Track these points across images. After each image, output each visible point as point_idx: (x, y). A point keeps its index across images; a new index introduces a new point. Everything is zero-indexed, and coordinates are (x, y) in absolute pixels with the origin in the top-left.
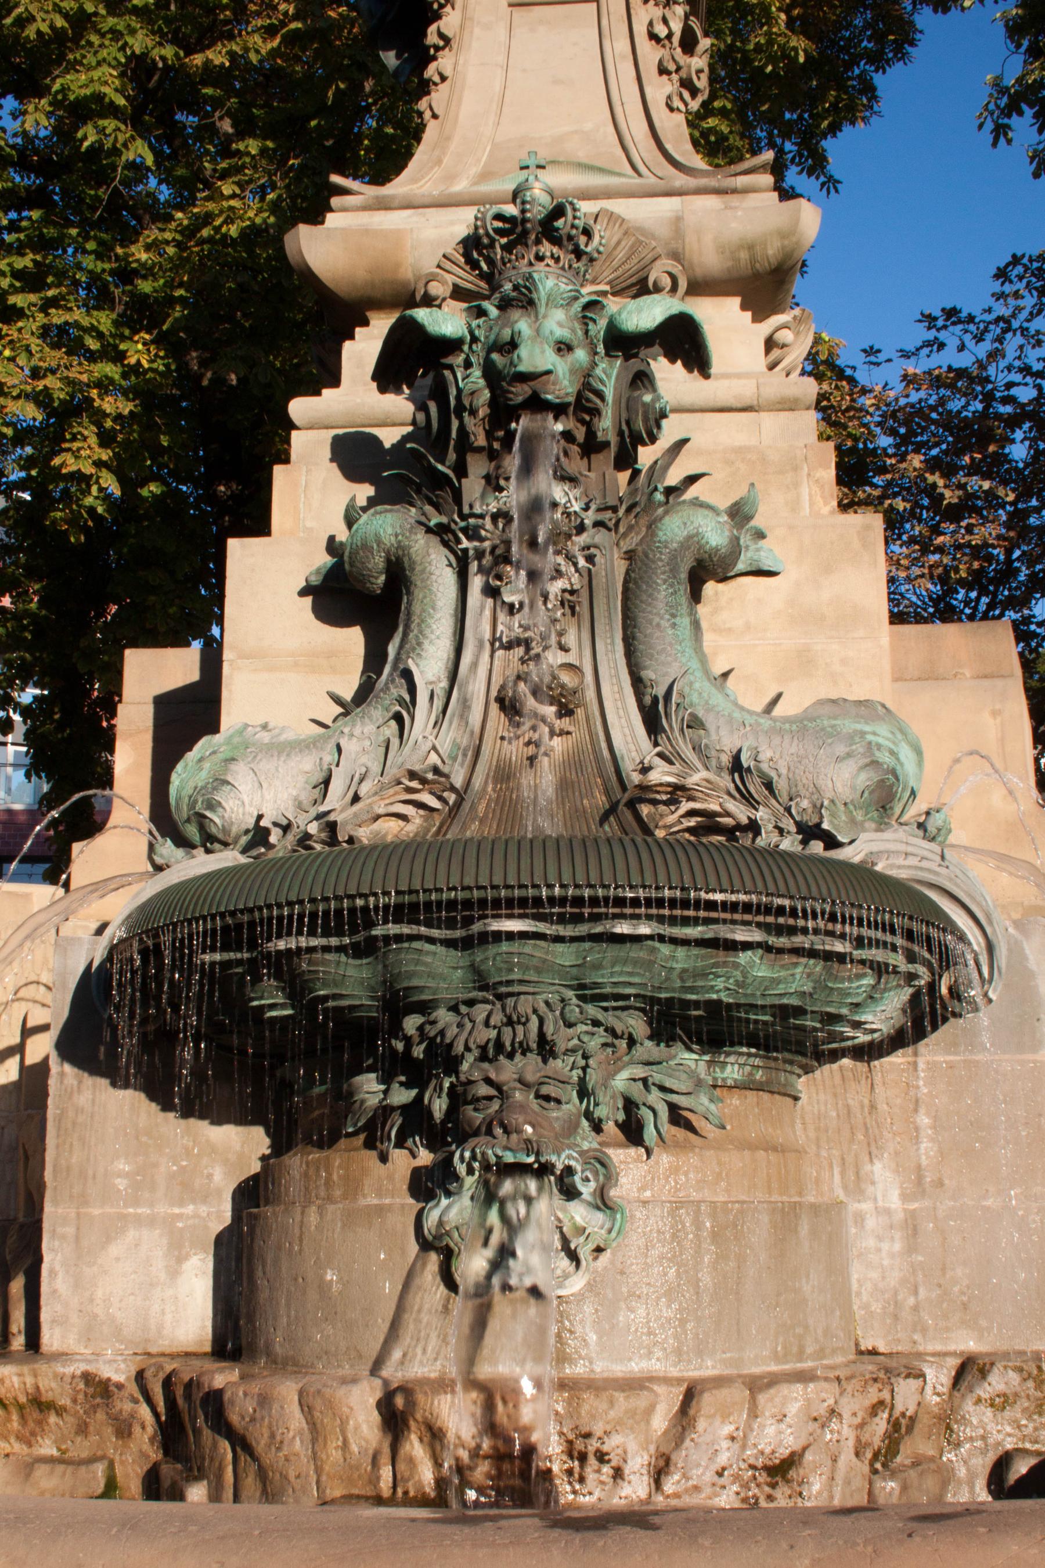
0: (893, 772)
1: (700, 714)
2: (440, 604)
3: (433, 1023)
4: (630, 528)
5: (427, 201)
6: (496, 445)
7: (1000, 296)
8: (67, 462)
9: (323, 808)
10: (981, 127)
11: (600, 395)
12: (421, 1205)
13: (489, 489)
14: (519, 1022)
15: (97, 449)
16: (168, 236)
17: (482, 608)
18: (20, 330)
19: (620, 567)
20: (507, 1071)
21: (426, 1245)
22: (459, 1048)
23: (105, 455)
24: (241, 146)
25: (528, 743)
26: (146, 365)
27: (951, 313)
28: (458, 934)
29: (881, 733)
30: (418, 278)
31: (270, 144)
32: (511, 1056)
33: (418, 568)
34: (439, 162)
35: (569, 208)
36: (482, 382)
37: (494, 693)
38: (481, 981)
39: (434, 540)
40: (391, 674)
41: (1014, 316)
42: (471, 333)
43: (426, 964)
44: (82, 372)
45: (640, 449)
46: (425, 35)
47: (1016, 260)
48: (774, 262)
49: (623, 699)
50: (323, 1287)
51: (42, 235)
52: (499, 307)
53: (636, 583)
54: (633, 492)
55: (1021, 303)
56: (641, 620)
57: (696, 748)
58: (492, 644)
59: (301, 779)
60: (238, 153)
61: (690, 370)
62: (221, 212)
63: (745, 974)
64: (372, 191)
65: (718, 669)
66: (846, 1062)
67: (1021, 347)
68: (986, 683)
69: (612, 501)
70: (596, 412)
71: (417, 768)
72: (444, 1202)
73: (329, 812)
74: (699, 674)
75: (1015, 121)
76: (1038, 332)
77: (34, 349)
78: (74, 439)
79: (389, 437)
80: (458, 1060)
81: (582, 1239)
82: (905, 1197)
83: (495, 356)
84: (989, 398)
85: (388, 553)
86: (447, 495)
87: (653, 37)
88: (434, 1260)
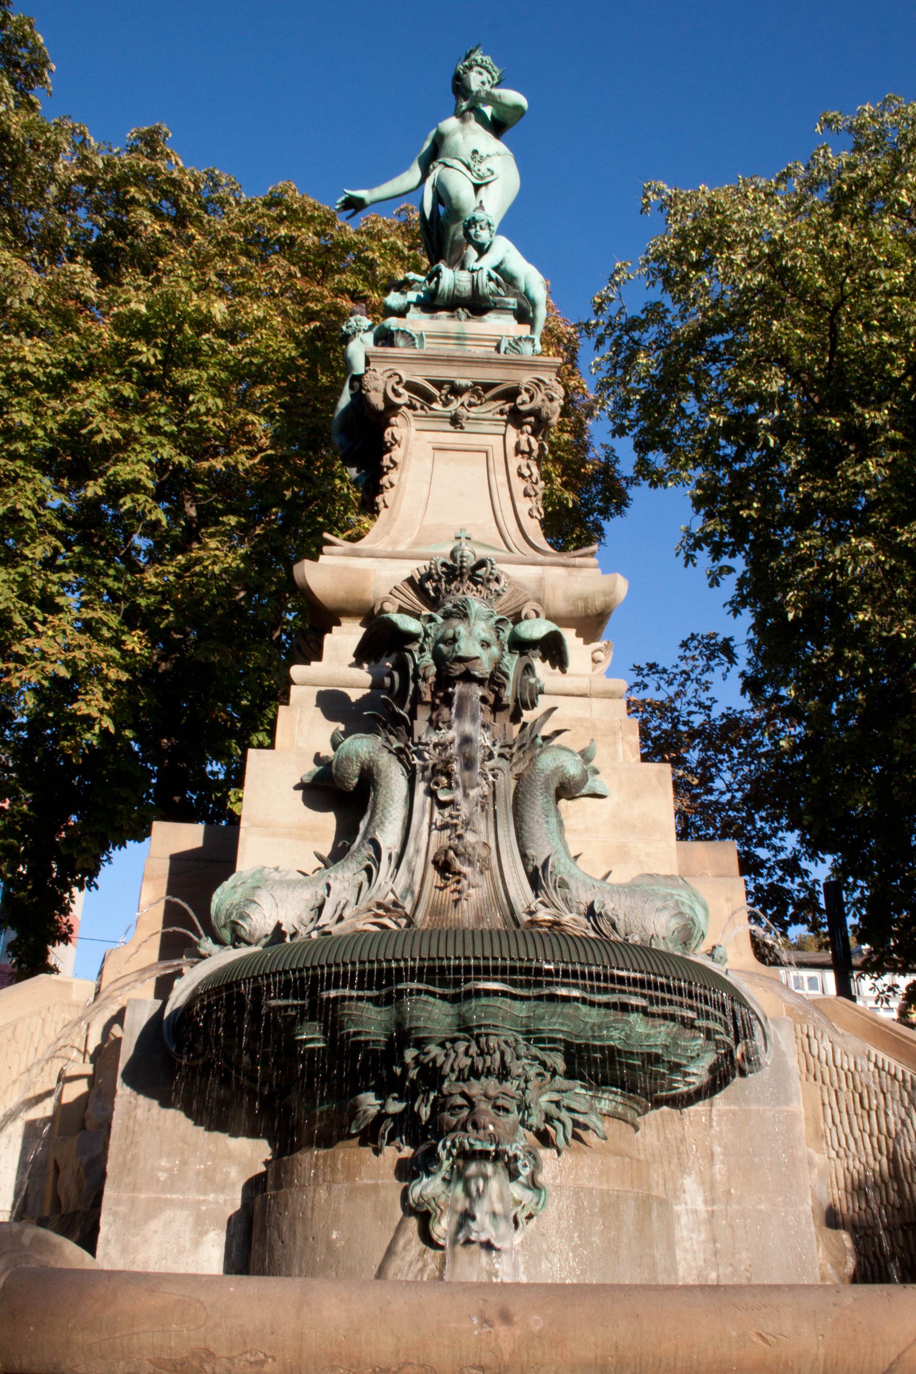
0: (692, 920)
1: (566, 878)
2: (396, 798)
3: (428, 1053)
4: (520, 759)
5: (384, 554)
6: (437, 701)
7: (683, 658)
8: (81, 708)
9: (320, 923)
10: (677, 554)
11: (506, 676)
12: (405, 1184)
13: (431, 729)
14: (488, 1053)
15: (102, 701)
16: (171, 569)
17: (424, 803)
18: (60, 619)
19: (513, 783)
20: (475, 1088)
21: (409, 1209)
22: (447, 1069)
23: (107, 706)
24: (225, 519)
25: (453, 892)
26: (138, 651)
27: (652, 666)
28: (450, 991)
29: (683, 896)
30: (377, 600)
31: (243, 520)
32: (478, 1078)
33: (383, 775)
34: (388, 533)
35: (489, 563)
36: (432, 662)
37: (431, 858)
38: (465, 1027)
39: (394, 758)
40: (361, 842)
41: (692, 671)
42: (425, 631)
43: (427, 1011)
44: (98, 650)
45: (524, 712)
46: (382, 460)
47: (693, 637)
48: (599, 609)
49: (515, 866)
50: (330, 1244)
51: (80, 562)
52: (443, 617)
53: (523, 794)
54: (522, 738)
55: (696, 663)
56: (526, 817)
57: (566, 901)
58: (430, 827)
59: (303, 904)
60: (224, 523)
61: (553, 667)
62: (209, 558)
63: (631, 1029)
64: (348, 545)
65: (573, 854)
66: (665, 1108)
67: (696, 691)
68: (721, 880)
69: (510, 743)
70: (503, 686)
71: (381, 900)
72: (425, 1180)
73: (324, 926)
74: (563, 854)
75: (698, 553)
76: (707, 682)
77: (68, 632)
78: (87, 693)
79: (355, 695)
80: (443, 1078)
81: (520, 1208)
82: (706, 1202)
83: (441, 646)
84: (675, 722)
85: (362, 764)
86: (402, 728)
87: (521, 475)
88: (413, 1223)
